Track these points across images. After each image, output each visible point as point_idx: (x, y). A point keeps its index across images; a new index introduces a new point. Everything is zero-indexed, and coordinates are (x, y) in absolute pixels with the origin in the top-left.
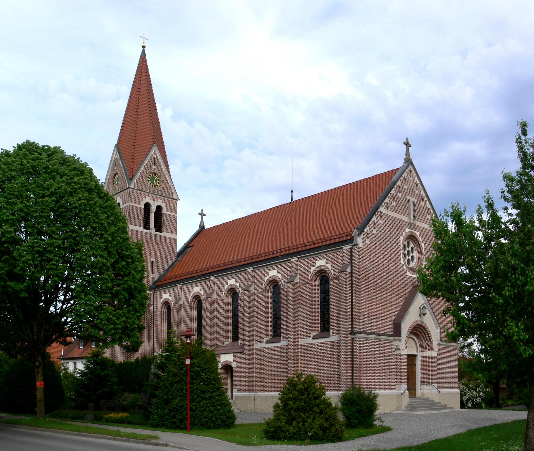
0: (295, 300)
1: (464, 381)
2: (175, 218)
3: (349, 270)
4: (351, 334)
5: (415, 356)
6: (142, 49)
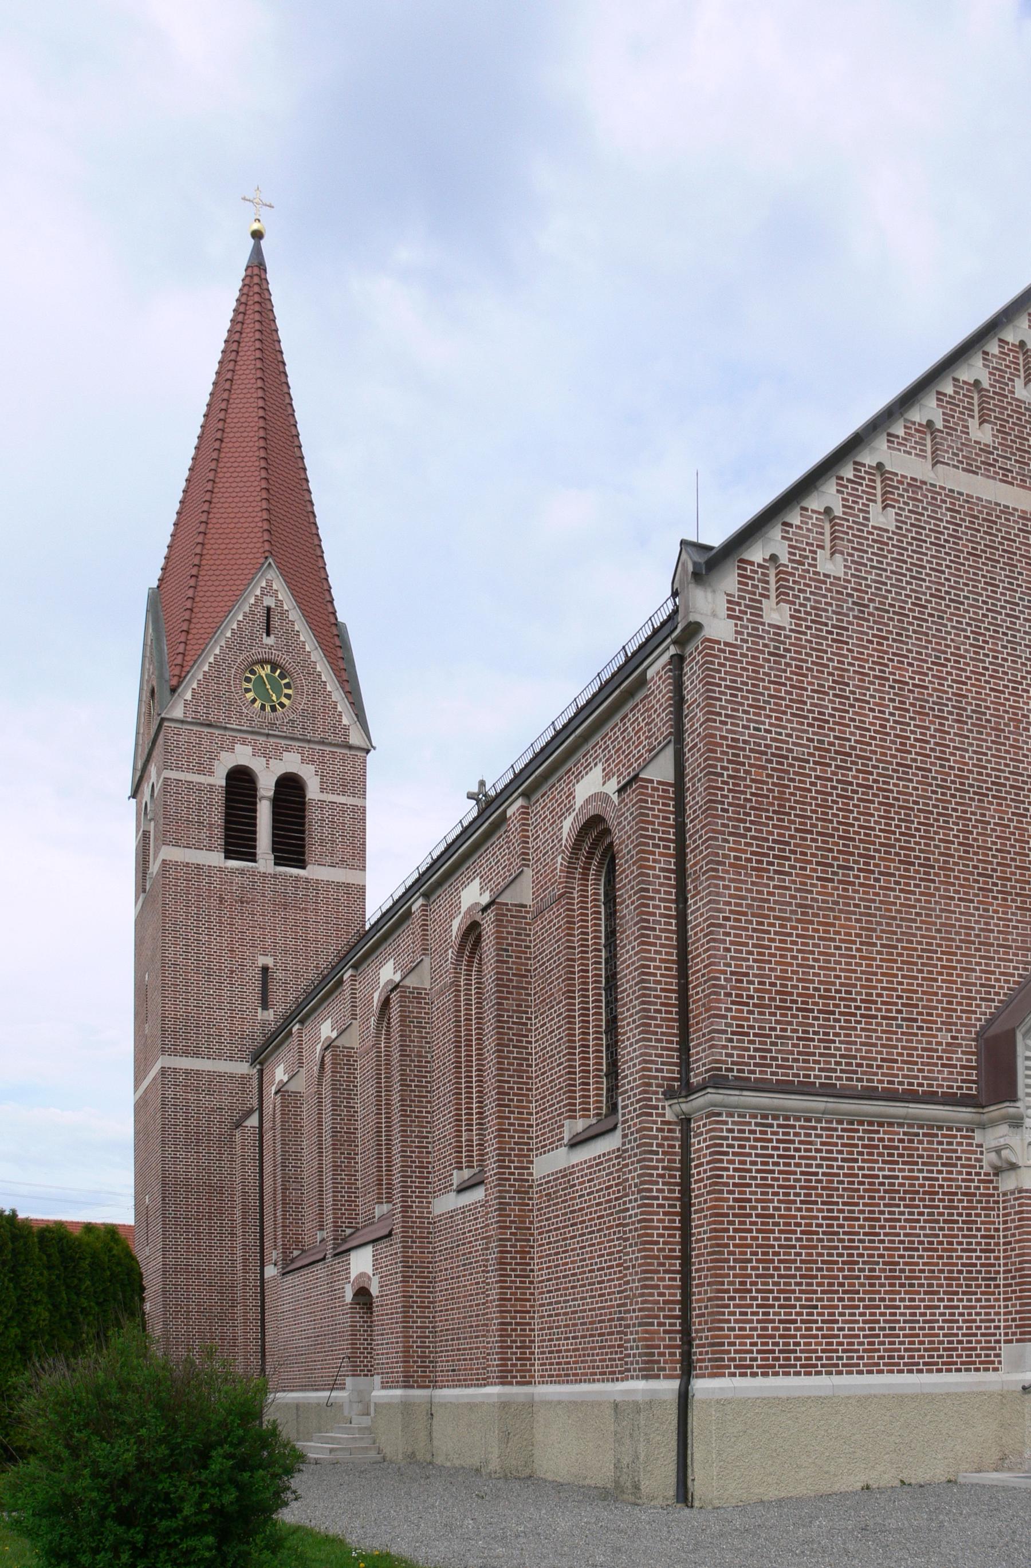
2: (359, 815)
3: (253, 1121)
4: (670, 1094)
6: (251, 242)
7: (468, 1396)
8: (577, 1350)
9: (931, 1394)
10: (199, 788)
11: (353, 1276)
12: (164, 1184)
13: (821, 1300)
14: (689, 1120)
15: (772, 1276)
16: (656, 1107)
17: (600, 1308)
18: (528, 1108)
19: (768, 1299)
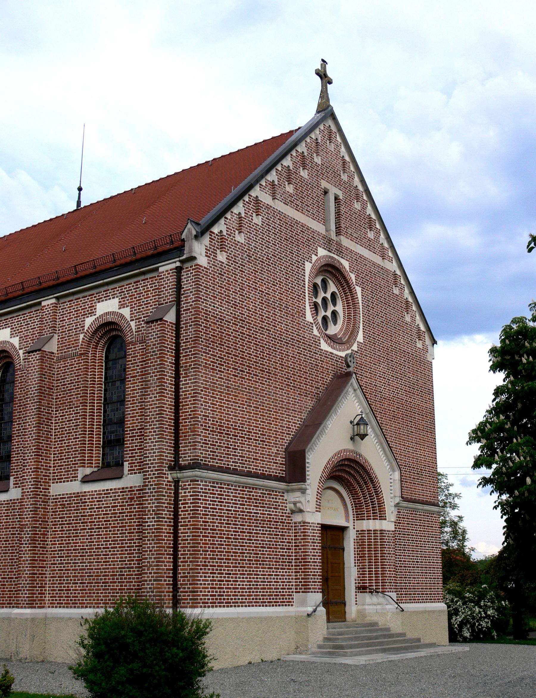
0: (44, 392)
1: (452, 585)
3: (171, 317)
4: (171, 468)
5: (343, 529)
14: (178, 481)
16: (165, 474)
18: (50, 457)
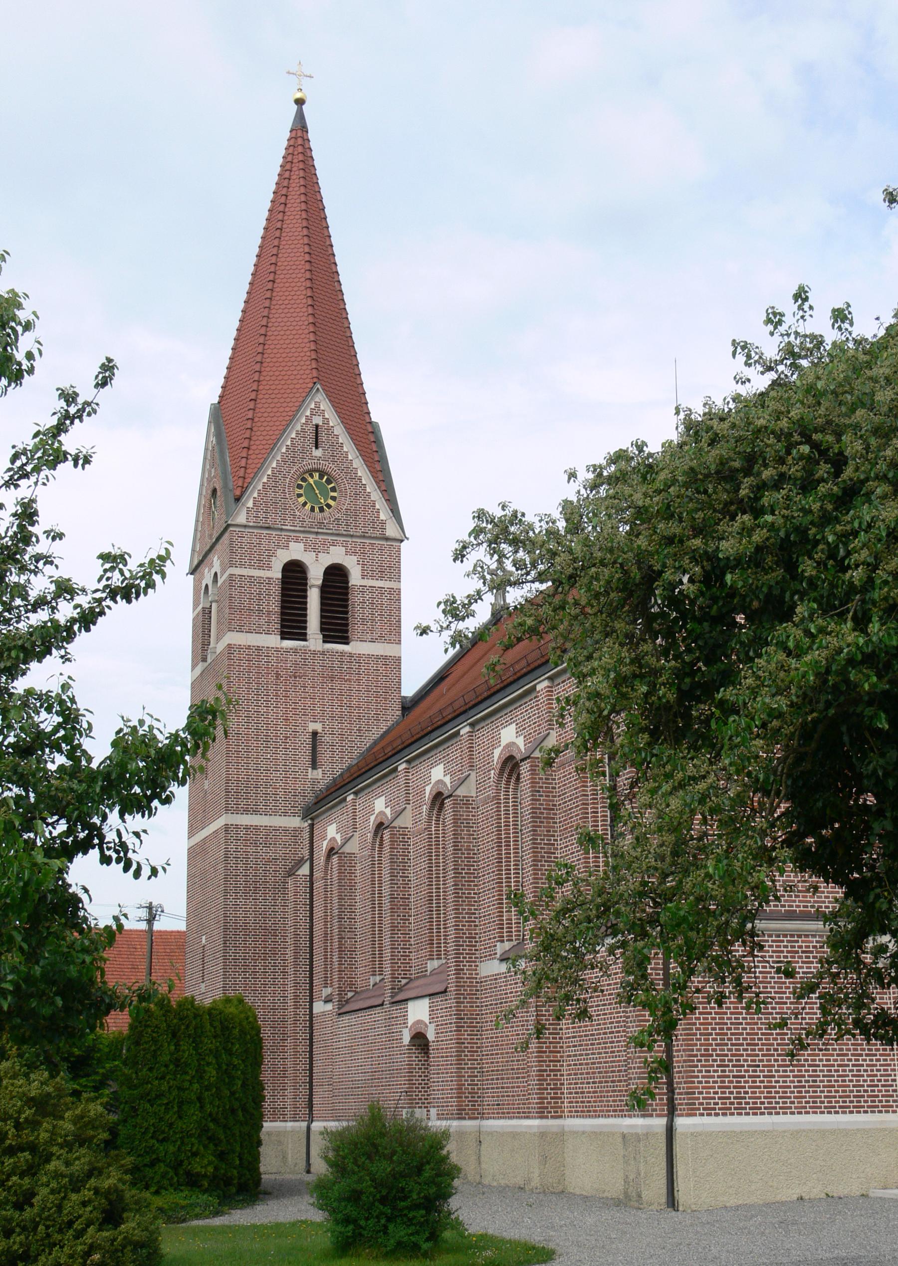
2: (395, 596)
3: (305, 870)
7: (510, 1126)
8: (596, 1092)
9: (845, 1130)
10: (260, 581)
11: (410, 1022)
12: (226, 929)
13: (762, 1061)
15: (727, 1045)
17: (611, 1062)
19: (724, 1061)
